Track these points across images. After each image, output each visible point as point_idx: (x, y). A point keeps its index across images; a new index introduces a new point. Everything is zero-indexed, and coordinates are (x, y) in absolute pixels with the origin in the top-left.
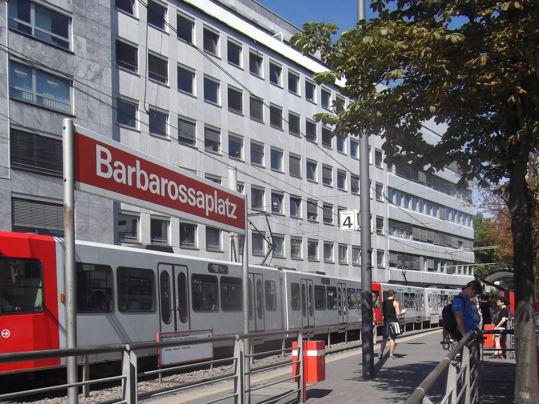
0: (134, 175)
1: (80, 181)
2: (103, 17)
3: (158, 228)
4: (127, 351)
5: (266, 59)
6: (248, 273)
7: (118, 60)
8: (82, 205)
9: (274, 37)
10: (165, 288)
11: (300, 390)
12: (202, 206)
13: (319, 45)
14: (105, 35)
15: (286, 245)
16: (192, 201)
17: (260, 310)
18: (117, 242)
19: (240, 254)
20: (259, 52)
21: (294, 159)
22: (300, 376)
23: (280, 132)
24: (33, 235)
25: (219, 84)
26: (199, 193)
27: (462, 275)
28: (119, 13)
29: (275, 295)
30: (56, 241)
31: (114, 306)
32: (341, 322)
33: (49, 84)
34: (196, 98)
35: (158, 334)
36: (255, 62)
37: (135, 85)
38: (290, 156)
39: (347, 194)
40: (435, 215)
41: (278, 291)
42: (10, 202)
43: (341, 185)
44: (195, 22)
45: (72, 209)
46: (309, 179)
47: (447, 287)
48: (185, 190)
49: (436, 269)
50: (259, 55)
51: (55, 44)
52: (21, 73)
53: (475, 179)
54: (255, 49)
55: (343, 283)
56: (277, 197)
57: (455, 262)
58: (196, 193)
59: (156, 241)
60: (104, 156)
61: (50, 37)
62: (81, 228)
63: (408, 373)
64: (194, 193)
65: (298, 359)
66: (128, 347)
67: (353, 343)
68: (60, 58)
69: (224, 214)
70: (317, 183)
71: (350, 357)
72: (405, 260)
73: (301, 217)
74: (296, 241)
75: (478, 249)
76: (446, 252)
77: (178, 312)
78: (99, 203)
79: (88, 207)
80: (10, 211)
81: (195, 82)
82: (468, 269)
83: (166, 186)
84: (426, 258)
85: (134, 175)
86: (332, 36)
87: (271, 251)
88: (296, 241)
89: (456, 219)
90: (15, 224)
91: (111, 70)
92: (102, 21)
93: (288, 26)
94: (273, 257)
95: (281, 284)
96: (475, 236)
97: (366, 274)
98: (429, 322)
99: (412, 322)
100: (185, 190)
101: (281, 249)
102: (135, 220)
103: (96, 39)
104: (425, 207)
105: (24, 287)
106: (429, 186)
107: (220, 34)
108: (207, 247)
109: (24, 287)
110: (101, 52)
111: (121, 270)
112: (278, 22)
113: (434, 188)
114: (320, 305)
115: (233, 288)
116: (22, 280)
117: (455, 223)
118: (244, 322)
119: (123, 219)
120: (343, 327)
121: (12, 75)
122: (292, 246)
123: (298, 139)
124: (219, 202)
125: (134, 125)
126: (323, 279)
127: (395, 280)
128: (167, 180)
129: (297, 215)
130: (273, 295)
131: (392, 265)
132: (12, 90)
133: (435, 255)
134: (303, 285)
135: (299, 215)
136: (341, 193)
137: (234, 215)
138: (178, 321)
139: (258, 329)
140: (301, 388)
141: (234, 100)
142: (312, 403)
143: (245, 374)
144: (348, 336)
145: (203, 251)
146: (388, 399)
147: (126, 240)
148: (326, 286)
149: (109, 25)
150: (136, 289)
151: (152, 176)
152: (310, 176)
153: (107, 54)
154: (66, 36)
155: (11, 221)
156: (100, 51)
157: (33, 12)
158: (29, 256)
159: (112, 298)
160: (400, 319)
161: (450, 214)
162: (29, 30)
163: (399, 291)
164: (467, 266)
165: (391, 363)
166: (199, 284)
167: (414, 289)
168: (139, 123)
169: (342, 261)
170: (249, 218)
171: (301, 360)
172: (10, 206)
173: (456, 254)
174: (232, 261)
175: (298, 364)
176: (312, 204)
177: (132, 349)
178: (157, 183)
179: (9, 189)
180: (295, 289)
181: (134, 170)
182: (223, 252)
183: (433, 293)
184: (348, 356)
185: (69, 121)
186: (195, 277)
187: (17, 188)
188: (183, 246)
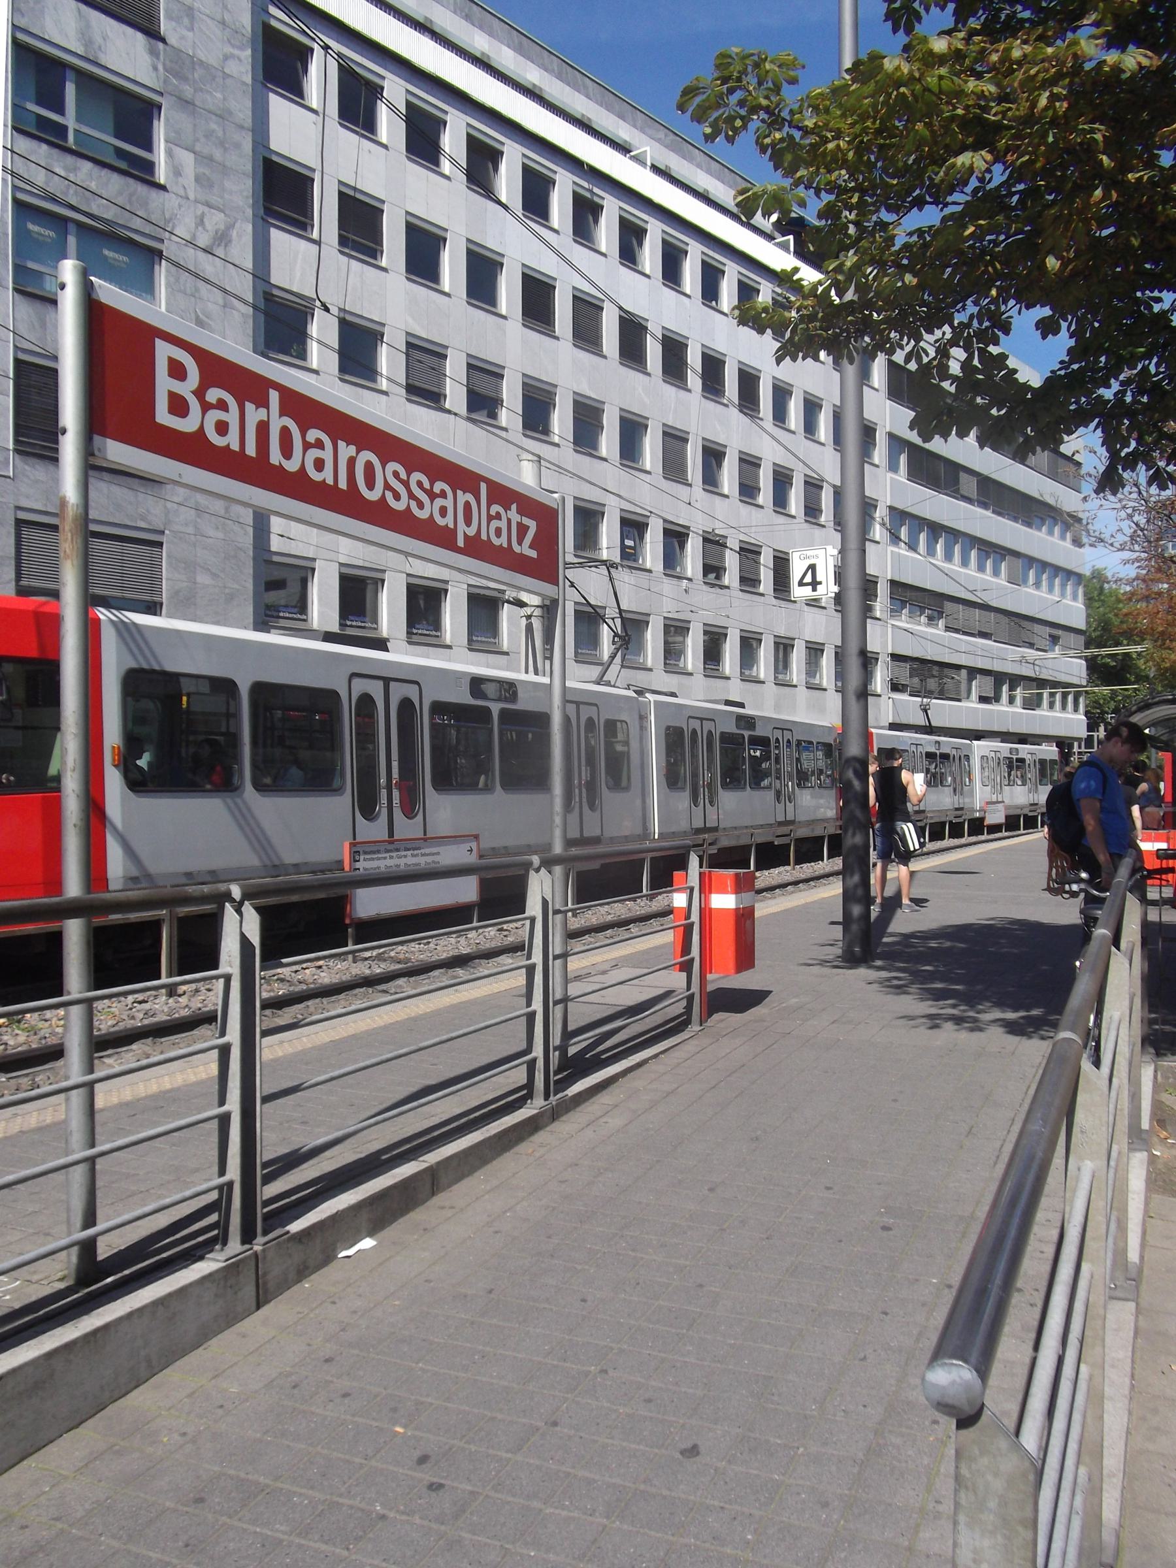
0: (263, 429)
1: (104, 434)
2: (233, 105)
3: (357, 593)
4: (233, 900)
5: (612, 208)
6: (565, 701)
7: (269, 205)
8: (181, 538)
9: (632, 158)
10: (365, 735)
11: (693, 995)
12: (448, 521)
13: (755, 109)
14: (237, 146)
15: (653, 638)
16: (421, 506)
17: (591, 787)
18: (262, 624)
19: (546, 658)
20: (596, 190)
21: (674, 439)
22: (693, 959)
23: (641, 376)
24: (45, 603)
25: (502, 265)
26: (439, 486)
27: (1057, 714)
28: (271, 95)
29: (628, 753)
30: (101, 617)
31: (241, 777)
32: (781, 818)
33: (106, 257)
34: (448, 295)
35: (347, 845)
36: (585, 213)
37: (304, 263)
38: (665, 433)
39: (795, 521)
40: (996, 573)
41: (634, 744)
42: (13, 531)
43: (780, 501)
44: (448, 118)
45: (81, 510)
46: (707, 487)
47: (1023, 739)
48: (403, 476)
49: (997, 699)
50: (596, 199)
51: (123, 165)
52: (42, 231)
53: (1141, 468)
54: (586, 185)
55: (784, 727)
56: (633, 526)
57: (1042, 683)
58: (432, 486)
59: (351, 626)
60: (177, 371)
61: (112, 149)
62: (177, 593)
63: (950, 949)
64: (427, 485)
65: (688, 917)
66: (236, 892)
67: (808, 869)
68: (134, 199)
69: (505, 545)
70: (727, 497)
71: (806, 906)
72: (926, 675)
73: (689, 574)
74: (675, 629)
75: (1096, 652)
76: (1023, 660)
77: (396, 794)
78: (220, 535)
79: (194, 545)
80: (12, 551)
81: (446, 257)
82: (1070, 698)
83: (351, 462)
84: (973, 672)
85: (263, 429)
86: (786, 90)
87: (618, 649)
88: (675, 629)
89: (1044, 583)
90: (24, 583)
91: (250, 227)
92: (230, 113)
93: (661, 134)
94: (622, 666)
95: (643, 728)
96: (1088, 623)
97: (854, 707)
98: (982, 819)
99: (943, 819)
100: (403, 476)
101: (640, 647)
102: (303, 573)
103: (218, 154)
104: (974, 554)
105: (24, 728)
106: (985, 506)
107: (505, 149)
108: (470, 641)
109: (24, 728)
110: (227, 184)
111: (259, 689)
112: (639, 123)
113: (994, 512)
114: (732, 778)
115: (530, 736)
116: (18, 712)
117: (1043, 593)
118: (553, 821)
119: (277, 574)
120: (785, 830)
121: (21, 236)
122: (666, 643)
123: (682, 393)
124: (493, 513)
125: (303, 355)
126: (740, 718)
127: (905, 721)
128: (352, 450)
129: (678, 569)
130: (622, 753)
131: (896, 687)
132: (19, 269)
133: (997, 666)
134: (694, 732)
135: (684, 569)
136: (781, 519)
137: (531, 547)
138: (398, 814)
139: (586, 834)
140: (695, 988)
141: (537, 298)
142: (721, 1025)
143: (556, 957)
144: (796, 851)
145: (461, 651)
146: (912, 1018)
147: (282, 623)
148: (746, 734)
149: (248, 123)
150: (296, 735)
151: (313, 435)
152: (710, 480)
153: (241, 190)
154: (149, 147)
155: (13, 575)
156: (227, 184)
157: (70, 90)
158: (34, 653)
159: (237, 758)
160: (917, 812)
161: (1032, 573)
162: (62, 130)
163: (913, 748)
164: (1069, 693)
165: (904, 922)
166: (450, 725)
167: (948, 743)
168: (315, 344)
169: (780, 677)
170: (570, 573)
171: (695, 917)
172: (12, 541)
173: (1049, 664)
174: (527, 672)
175: (688, 929)
176: (713, 543)
177: (246, 896)
178: (327, 455)
179: (11, 501)
180: (674, 739)
181: (262, 414)
182: (507, 654)
183: (993, 754)
184: (802, 901)
185: (75, 266)
186: (438, 708)
187: (27, 497)
188: (415, 639)
